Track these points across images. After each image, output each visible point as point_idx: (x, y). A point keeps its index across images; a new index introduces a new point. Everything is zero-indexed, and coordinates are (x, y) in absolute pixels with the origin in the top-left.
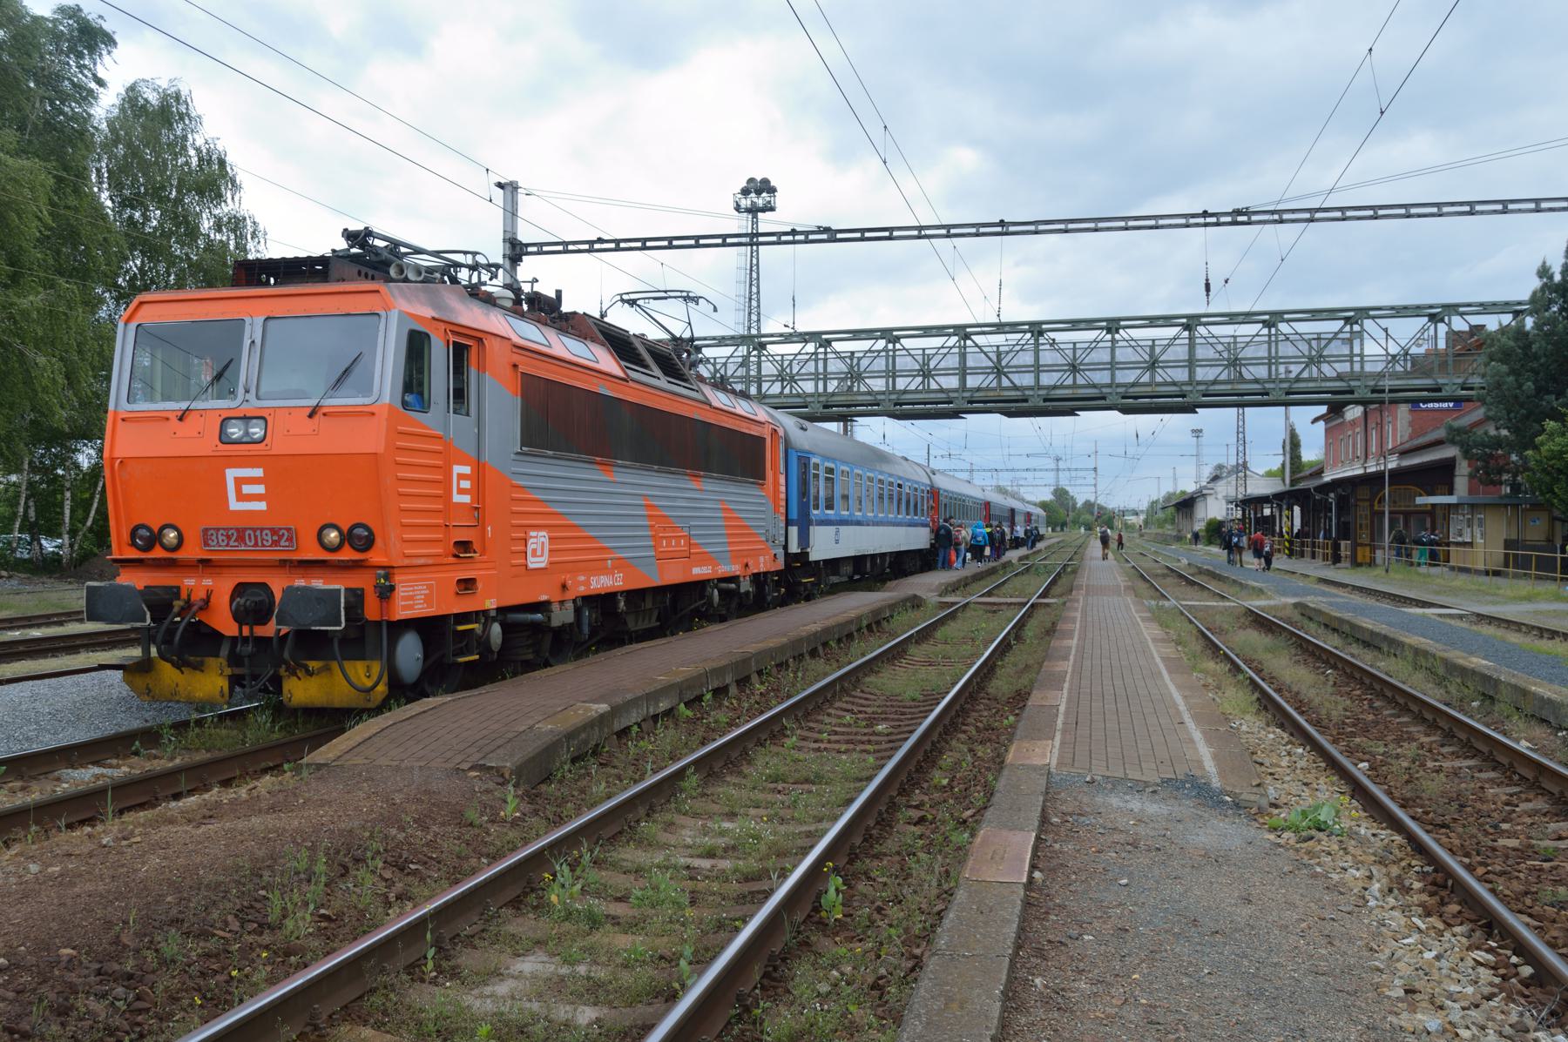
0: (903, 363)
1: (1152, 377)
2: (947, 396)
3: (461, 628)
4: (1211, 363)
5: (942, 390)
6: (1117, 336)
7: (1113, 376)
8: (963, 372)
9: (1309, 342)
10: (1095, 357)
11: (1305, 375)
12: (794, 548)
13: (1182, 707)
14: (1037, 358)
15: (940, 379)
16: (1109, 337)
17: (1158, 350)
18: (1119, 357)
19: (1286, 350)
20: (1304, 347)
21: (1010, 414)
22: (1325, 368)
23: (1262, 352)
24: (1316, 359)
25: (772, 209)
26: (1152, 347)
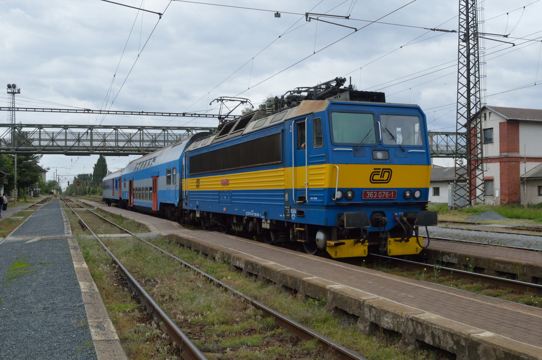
0: (95, 137)
1: (79, 144)
2: (87, 148)
3: (303, 229)
4: (45, 140)
5: (59, 146)
6: (67, 131)
7: (66, 143)
8: (92, 140)
9: (152, 136)
10: (84, 137)
11: (126, 145)
12: (440, 217)
13: (431, 289)
14: (66, 137)
15: (84, 142)
16: (64, 131)
17: (81, 136)
18: (42, 137)
19: (146, 138)
20: (151, 138)
21: (67, 154)
22: (157, 143)
23: (113, 138)
24: (130, 141)
25: (19, 93)
26: (79, 135)
